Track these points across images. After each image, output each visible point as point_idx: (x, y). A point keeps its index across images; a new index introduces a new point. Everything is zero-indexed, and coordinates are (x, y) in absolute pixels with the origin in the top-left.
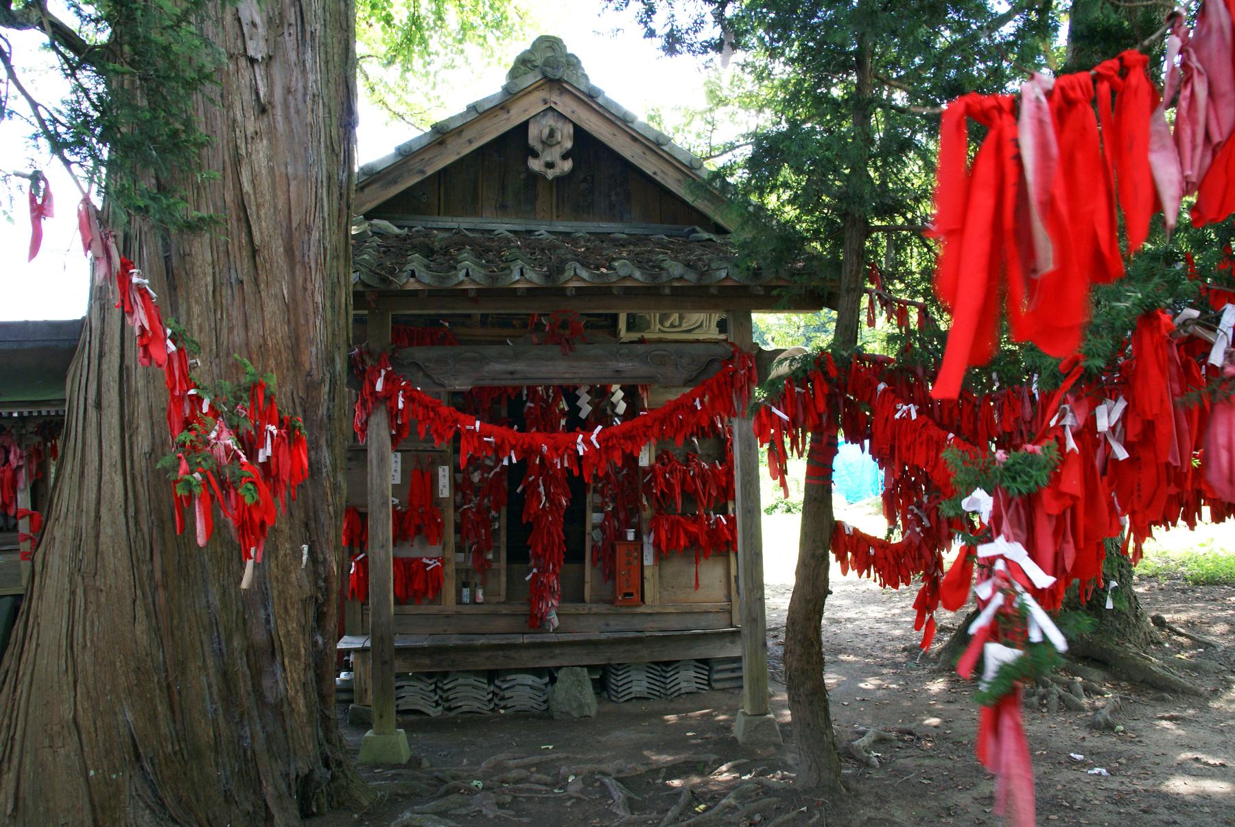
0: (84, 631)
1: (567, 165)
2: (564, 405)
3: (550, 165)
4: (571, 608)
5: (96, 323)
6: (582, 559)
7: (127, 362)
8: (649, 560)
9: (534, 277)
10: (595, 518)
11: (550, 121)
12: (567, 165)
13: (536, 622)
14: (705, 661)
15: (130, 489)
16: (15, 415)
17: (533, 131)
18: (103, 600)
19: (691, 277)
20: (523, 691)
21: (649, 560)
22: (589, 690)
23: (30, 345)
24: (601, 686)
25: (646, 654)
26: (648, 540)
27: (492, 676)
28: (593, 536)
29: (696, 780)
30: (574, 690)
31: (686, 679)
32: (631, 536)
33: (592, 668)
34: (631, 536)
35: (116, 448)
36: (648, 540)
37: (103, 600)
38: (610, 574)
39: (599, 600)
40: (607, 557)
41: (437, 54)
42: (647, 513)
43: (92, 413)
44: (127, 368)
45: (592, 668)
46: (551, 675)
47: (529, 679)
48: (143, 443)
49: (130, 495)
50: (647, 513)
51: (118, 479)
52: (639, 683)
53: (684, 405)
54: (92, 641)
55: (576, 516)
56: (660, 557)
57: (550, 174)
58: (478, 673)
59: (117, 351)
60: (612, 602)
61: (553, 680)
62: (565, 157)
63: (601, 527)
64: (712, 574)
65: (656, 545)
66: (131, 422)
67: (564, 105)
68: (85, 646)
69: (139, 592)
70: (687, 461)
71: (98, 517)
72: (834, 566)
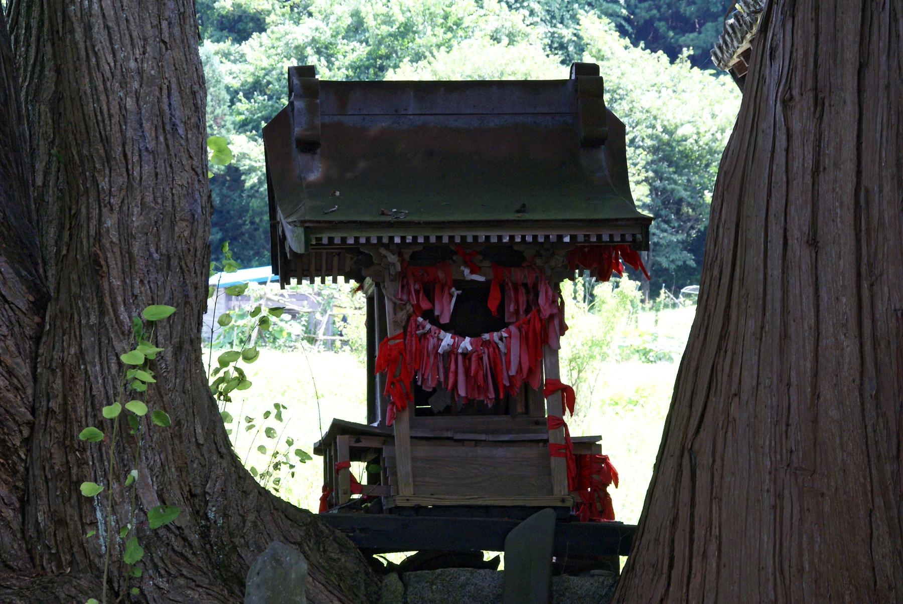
0: (800, 546)
5: (641, 529)
7: (865, 182)
15: (869, 359)
16: (567, 239)
18: (827, 508)
23: (276, 114)
35: (847, 303)
37: (827, 508)
41: (445, 33)
43: (799, 251)
44: (867, 191)
49: (870, 365)
51: (850, 346)
54: (812, 563)
59: (849, 166)
66: (870, 265)
68: (801, 570)
69: (879, 501)
71: (816, 395)
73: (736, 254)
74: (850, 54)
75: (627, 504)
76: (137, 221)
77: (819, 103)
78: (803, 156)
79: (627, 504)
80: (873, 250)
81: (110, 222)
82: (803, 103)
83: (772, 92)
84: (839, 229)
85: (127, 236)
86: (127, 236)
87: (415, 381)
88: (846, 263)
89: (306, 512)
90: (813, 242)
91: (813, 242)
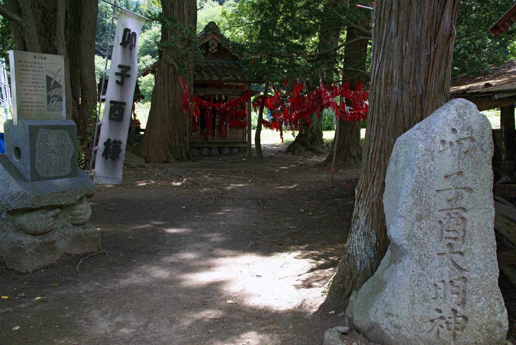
1: (216, 50)
2: (213, 97)
3: (213, 50)
4: (213, 137)
6: (215, 128)
8: (228, 128)
9: (217, 78)
10: (217, 120)
11: (213, 41)
12: (216, 50)
13: (206, 139)
14: (239, 148)
17: (210, 43)
19: (242, 79)
20: (205, 151)
21: (228, 128)
22: (218, 152)
24: (219, 152)
25: (228, 145)
26: (228, 125)
27: (199, 148)
28: (217, 123)
29: (256, 57)
30: (215, 151)
31: (235, 151)
32: (225, 124)
33: (218, 148)
34: (225, 124)
36: (228, 125)
38: (220, 131)
39: (217, 136)
40: (220, 128)
42: (228, 119)
43: (162, 100)
45: (218, 148)
46: (210, 149)
47: (206, 149)
48: (171, 104)
50: (228, 119)
52: (227, 151)
53: (239, 99)
55: (214, 120)
56: (230, 128)
57: (213, 52)
58: (197, 148)
60: (221, 136)
61: (211, 150)
62: (216, 48)
63: (218, 122)
64: (240, 131)
65: (230, 126)
67: (216, 38)
70: (236, 109)
72: (263, 126)
73: (155, 98)
74: (167, 80)
75: (143, 126)
76: (91, 97)
77: (164, 85)
78: (162, 90)
79: (143, 126)
80: (181, 15)
81: (88, 97)
82: (162, 85)
83: (159, 84)
84: (166, 98)
85: (90, 98)
86: (90, 98)
87: (131, 118)
88: (167, 101)
89: (360, 136)
90: (164, 99)
91: (164, 99)
